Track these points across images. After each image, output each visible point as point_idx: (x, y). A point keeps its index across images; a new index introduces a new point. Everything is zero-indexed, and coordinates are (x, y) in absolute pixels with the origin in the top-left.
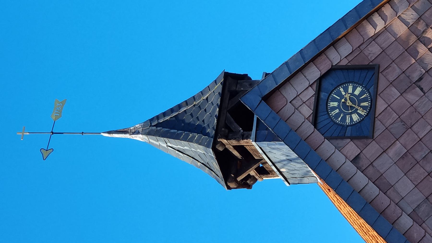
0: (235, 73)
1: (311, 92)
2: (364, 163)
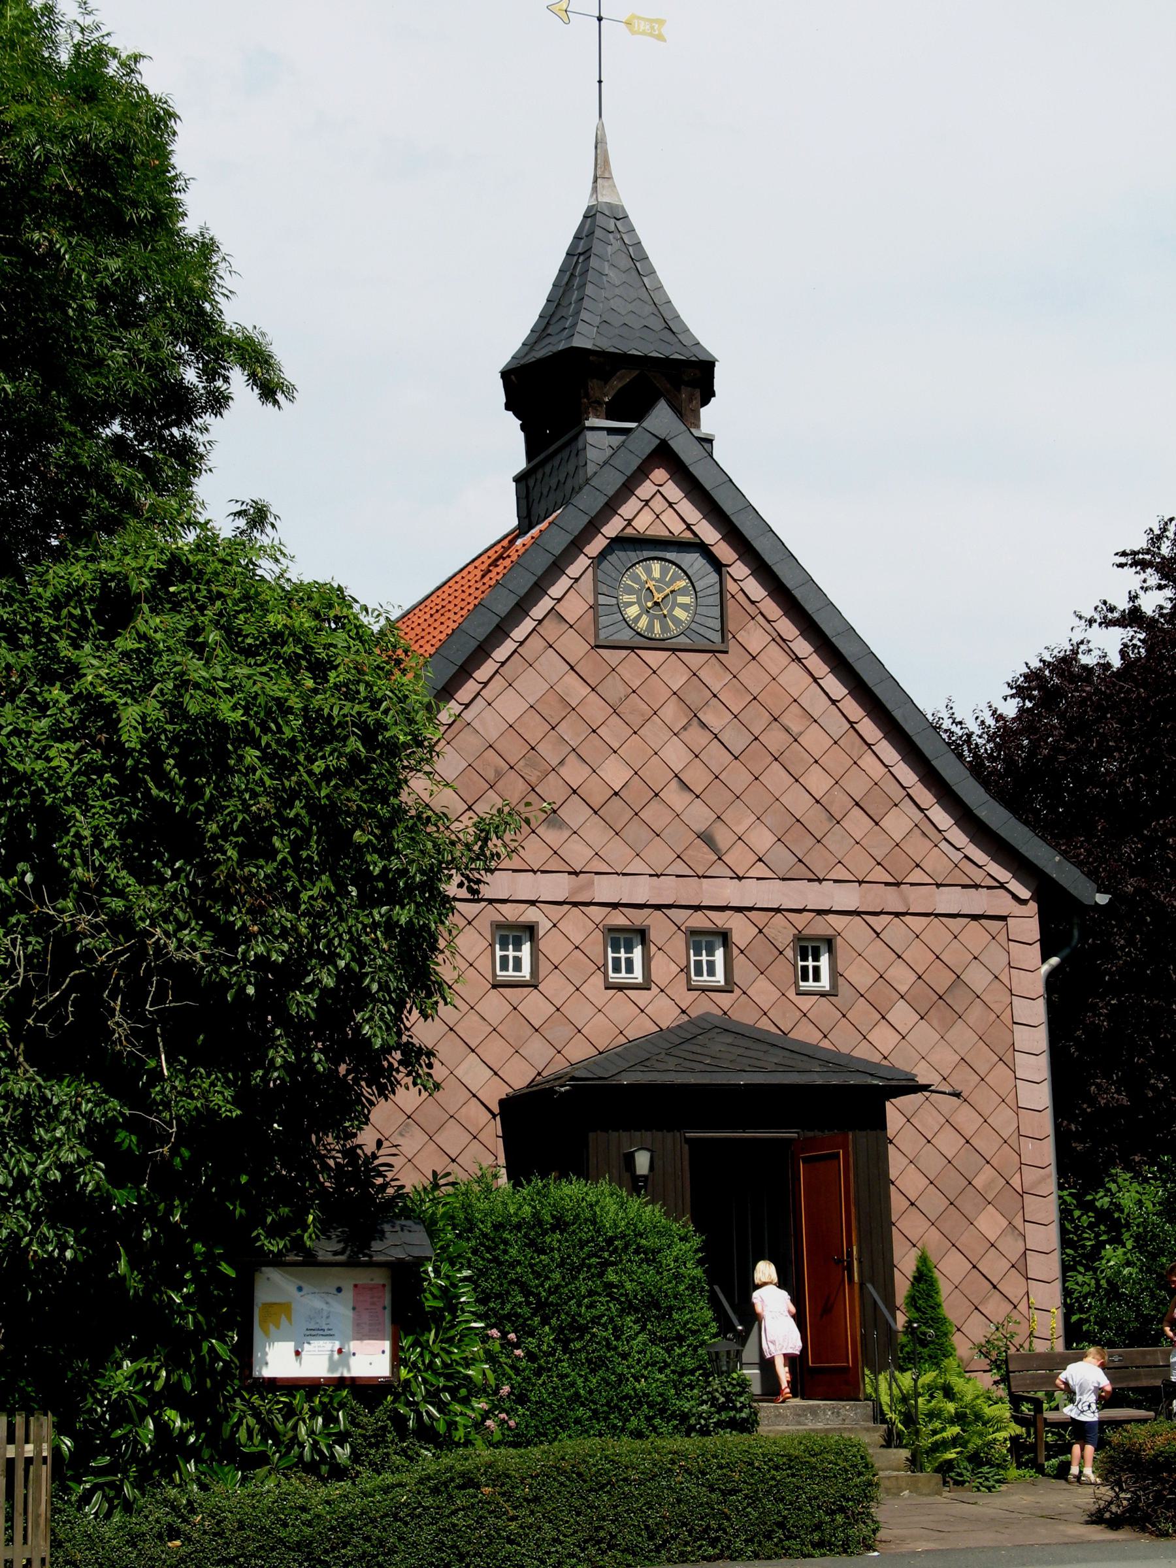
0: (483, 668)
1: (677, 528)
2: (551, 629)
